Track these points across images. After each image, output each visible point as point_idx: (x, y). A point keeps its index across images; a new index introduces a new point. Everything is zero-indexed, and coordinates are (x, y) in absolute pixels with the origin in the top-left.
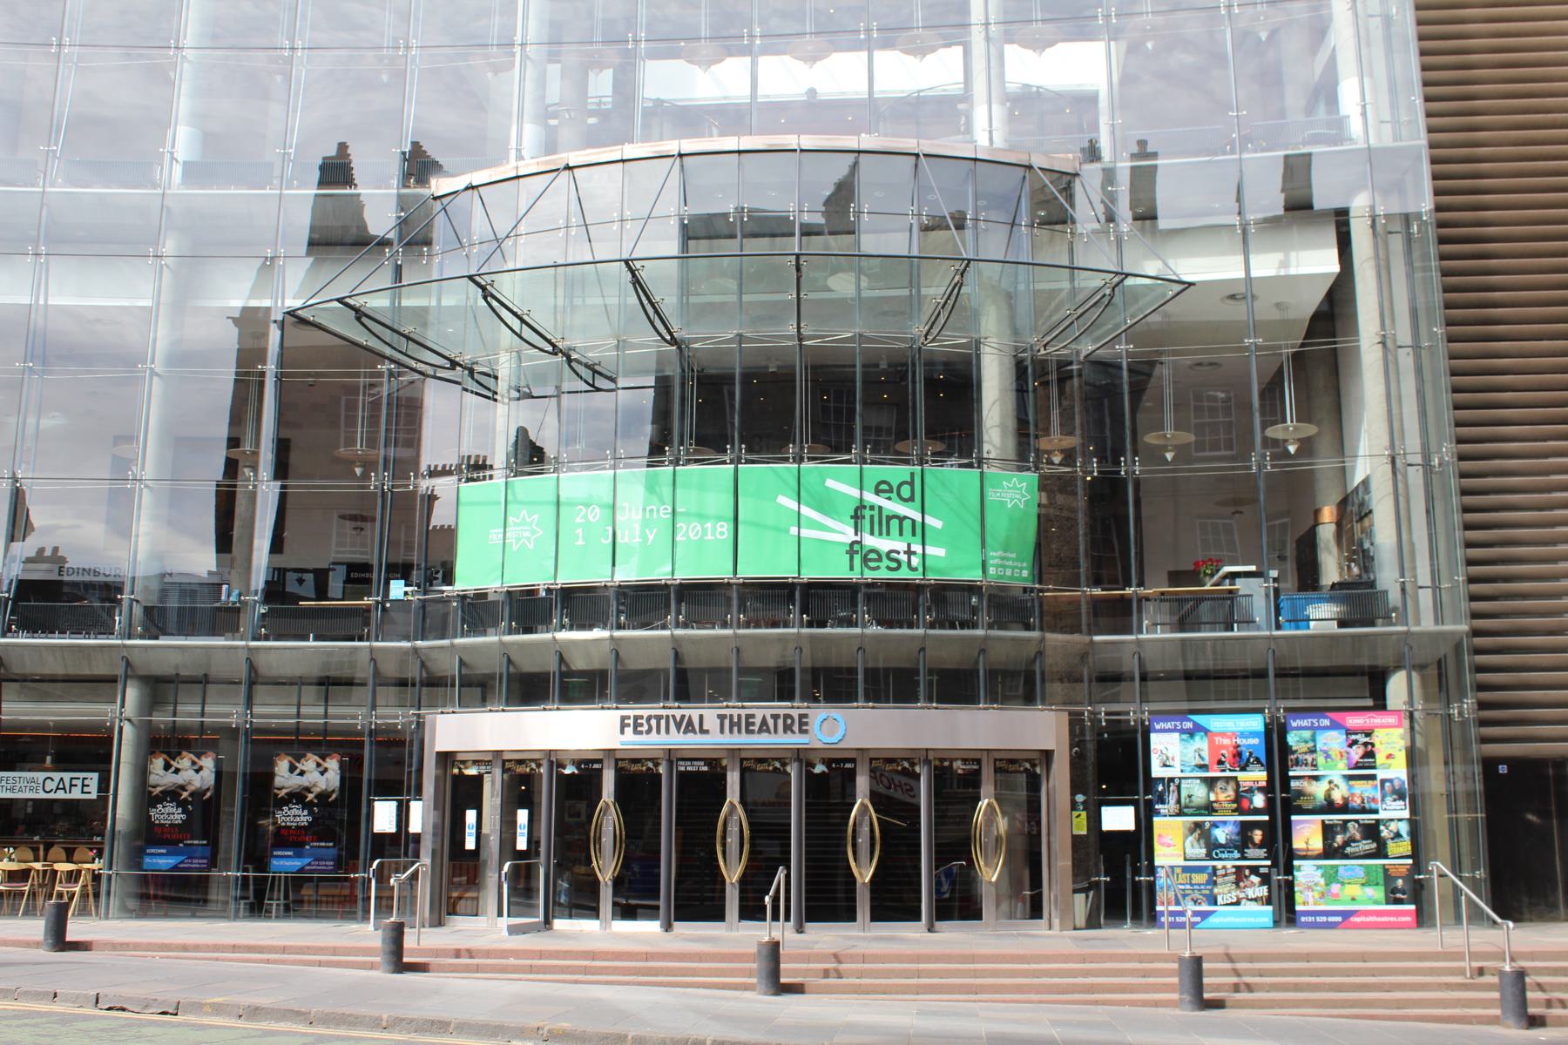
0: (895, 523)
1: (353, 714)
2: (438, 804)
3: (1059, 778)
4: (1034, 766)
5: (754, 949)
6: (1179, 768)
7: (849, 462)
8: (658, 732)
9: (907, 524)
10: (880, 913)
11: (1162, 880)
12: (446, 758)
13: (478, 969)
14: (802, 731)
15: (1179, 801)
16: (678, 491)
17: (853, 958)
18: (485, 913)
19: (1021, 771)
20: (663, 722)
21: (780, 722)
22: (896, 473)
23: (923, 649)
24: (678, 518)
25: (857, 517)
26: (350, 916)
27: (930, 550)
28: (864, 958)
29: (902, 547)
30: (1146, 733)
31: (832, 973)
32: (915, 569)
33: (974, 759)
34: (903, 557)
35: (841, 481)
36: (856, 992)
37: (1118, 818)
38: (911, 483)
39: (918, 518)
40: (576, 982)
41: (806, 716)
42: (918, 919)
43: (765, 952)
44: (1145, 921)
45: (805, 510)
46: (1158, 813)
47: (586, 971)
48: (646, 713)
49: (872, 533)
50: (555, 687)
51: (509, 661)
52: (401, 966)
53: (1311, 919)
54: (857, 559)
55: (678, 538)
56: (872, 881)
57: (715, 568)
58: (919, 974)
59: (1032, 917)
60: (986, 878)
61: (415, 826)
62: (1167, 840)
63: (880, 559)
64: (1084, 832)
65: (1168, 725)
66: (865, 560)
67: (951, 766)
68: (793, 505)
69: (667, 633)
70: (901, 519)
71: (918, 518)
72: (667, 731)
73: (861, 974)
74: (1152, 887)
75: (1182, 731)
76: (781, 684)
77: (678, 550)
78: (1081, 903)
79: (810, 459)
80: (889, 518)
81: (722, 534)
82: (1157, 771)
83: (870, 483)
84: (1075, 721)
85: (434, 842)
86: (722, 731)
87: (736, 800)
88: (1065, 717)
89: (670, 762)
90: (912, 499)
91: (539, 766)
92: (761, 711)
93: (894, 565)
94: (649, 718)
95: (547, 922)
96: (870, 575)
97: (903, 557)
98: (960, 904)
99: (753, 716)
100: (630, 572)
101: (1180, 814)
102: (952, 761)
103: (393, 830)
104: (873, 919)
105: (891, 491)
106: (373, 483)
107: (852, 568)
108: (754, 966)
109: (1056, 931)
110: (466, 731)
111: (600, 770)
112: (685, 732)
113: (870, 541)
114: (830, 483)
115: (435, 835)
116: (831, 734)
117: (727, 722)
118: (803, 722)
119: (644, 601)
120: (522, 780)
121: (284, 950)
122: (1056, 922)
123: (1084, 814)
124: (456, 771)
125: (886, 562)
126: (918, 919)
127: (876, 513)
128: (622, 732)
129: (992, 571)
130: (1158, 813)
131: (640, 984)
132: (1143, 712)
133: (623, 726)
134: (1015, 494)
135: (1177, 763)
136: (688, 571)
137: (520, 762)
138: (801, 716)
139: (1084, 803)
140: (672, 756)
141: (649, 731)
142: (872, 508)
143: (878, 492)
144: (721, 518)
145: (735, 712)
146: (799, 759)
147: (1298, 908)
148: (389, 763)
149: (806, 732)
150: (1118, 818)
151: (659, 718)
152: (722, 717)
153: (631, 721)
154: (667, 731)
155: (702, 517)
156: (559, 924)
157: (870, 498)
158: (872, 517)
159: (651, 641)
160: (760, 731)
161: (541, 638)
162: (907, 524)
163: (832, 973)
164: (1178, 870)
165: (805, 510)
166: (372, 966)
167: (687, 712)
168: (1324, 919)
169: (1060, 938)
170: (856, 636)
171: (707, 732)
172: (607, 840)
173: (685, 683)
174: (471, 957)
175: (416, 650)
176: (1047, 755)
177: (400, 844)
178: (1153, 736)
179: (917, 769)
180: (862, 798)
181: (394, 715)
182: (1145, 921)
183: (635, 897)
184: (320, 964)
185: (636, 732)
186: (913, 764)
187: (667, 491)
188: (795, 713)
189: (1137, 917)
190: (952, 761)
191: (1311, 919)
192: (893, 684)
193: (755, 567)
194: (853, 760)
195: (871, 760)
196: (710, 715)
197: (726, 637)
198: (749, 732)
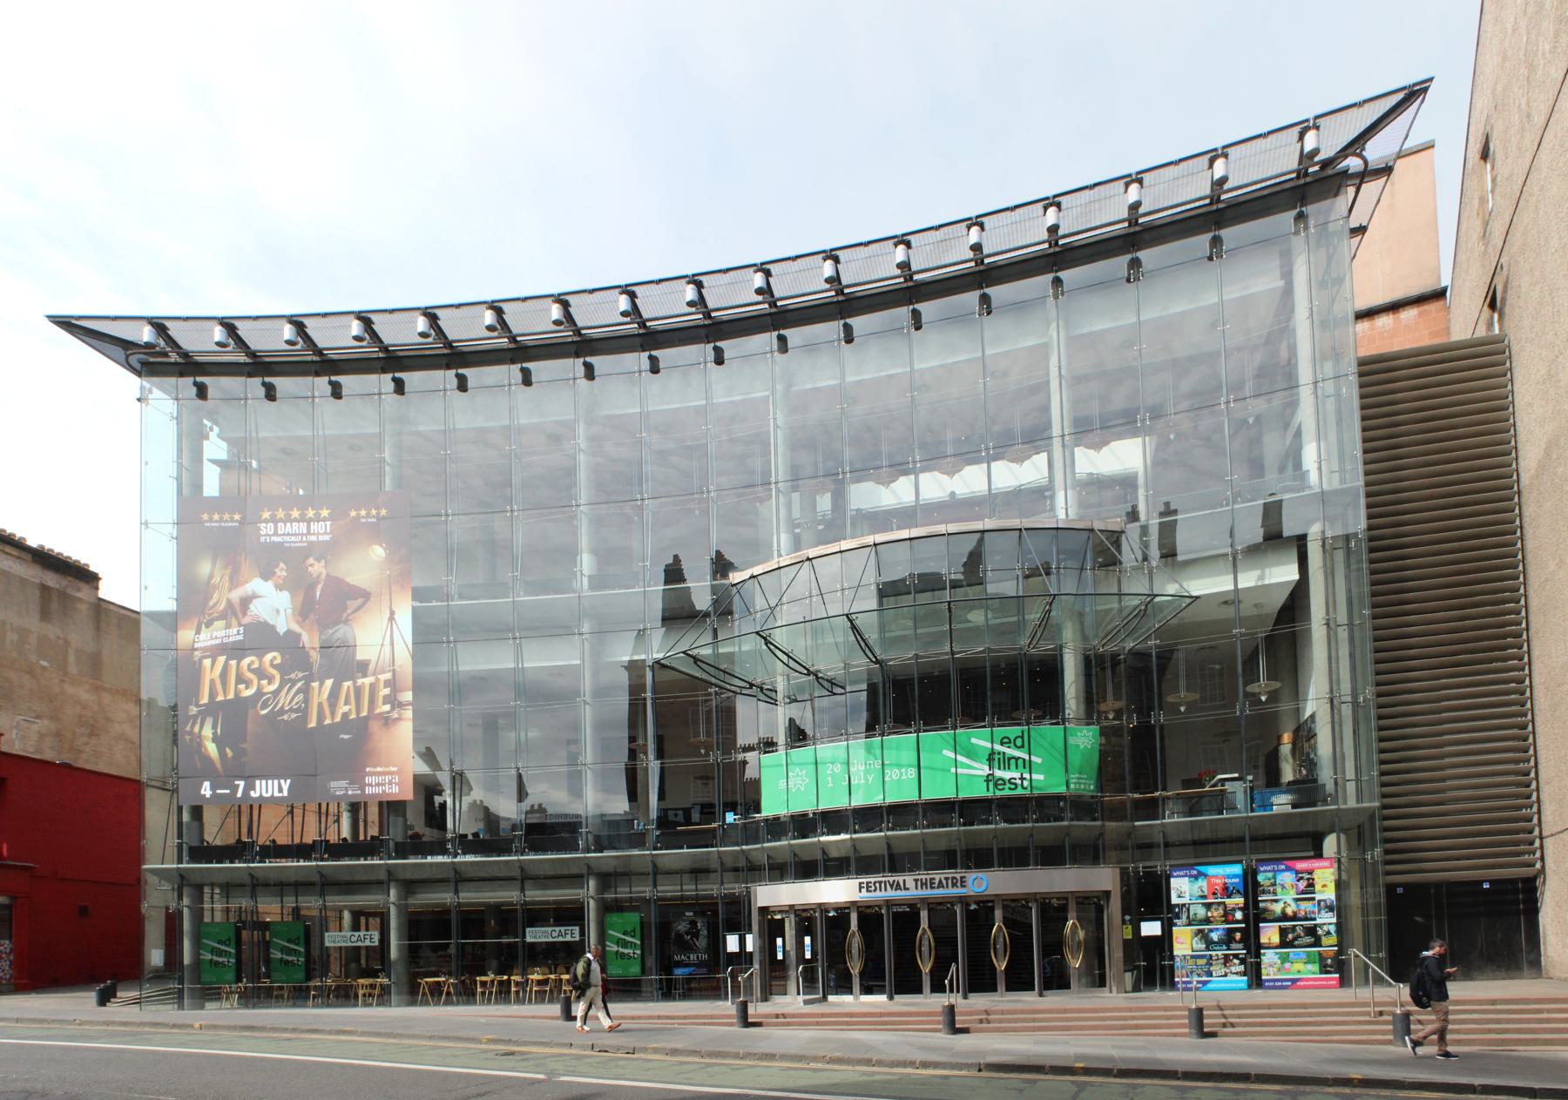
0: (1013, 762)
2: (761, 935)
10: (1011, 987)
11: (1178, 963)
13: (788, 1024)
17: (996, 1013)
19: (1092, 905)
22: (1013, 731)
25: (990, 759)
27: (1035, 776)
28: (1002, 1013)
29: (1018, 775)
33: (1064, 897)
35: (980, 739)
37: (1151, 928)
47: (847, 1023)
57: (908, 795)
61: (749, 948)
66: (996, 785)
70: (1017, 759)
73: (1001, 1021)
74: (1172, 968)
76: (948, 859)
82: (1175, 900)
83: (997, 738)
96: (998, 793)
104: (1008, 990)
109: (1114, 994)
110: (775, 895)
113: (998, 773)
114: (973, 740)
119: (868, 816)
120: (806, 918)
140: (889, 903)
143: (1002, 744)
148: (736, 915)
150: (1151, 928)
155: (899, 766)
156: (831, 998)
157: (998, 747)
172: (855, 951)
176: (1107, 894)
180: (924, 923)
187: (878, 752)
192: (1014, 857)
196: (909, 879)
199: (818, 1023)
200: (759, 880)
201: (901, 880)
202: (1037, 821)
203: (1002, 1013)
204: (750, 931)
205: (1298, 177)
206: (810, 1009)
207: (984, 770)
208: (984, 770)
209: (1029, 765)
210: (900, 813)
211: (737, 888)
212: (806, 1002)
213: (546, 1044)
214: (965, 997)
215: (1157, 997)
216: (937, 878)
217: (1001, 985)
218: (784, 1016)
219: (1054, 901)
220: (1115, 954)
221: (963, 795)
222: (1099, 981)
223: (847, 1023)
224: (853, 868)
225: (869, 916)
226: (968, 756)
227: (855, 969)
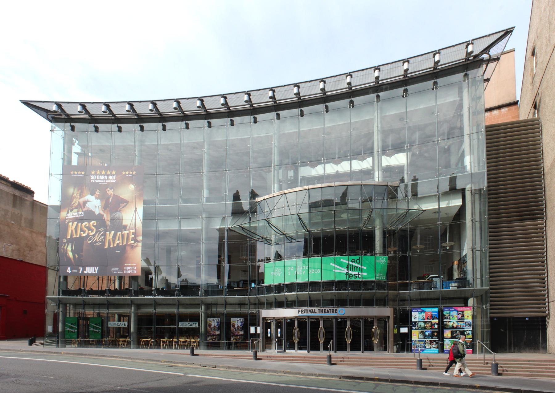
0: (356, 268)
2: (263, 328)
3: (391, 321)
10: (352, 349)
12: (264, 319)
13: (272, 360)
17: (346, 358)
19: (382, 321)
22: (356, 257)
25: (347, 267)
28: (349, 358)
29: (357, 273)
33: (372, 318)
35: (344, 259)
37: (404, 330)
47: (292, 360)
57: (317, 279)
61: (258, 332)
66: (349, 276)
68: (334, 265)
70: (357, 267)
73: (348, 361)
74: (411, 344)
76: (331, 302)
82: (413, 320)
83: (350, 260)
84: (395, 310)
96: (350, 279)
101: (418, 329)
113: (350, 272)
114: (342, 260)
119: (303, 286)
120: (279, 322)
133: (299, 312)
136: (312, 280)
140: (309, 318)
143: (352, 262)
148: (253, 320)
150: (404, 330)
155: (314, 268)
156: (287, 351)
157: (350, 263)
166: (251, 359)
172: (296, 335)
173: (312, 303)
176: (389, 317)
177: (256, 335)
187: (307, 263)
188: (334, 309)
193: (325, 279)
196: (317, 309)
200: (262, 308)
201: (313, 309)
205: (465, 61)
209: (361, 270)
210: (314, 285)
211: (254, 310)
214: (335, 352)
215: (405, 355)
216: (327, 309)
217: (349, 348)
219: (369, 319)
221: (338, 279)
223: (292, 360)
225: (302, 322)
227: (296, 341)
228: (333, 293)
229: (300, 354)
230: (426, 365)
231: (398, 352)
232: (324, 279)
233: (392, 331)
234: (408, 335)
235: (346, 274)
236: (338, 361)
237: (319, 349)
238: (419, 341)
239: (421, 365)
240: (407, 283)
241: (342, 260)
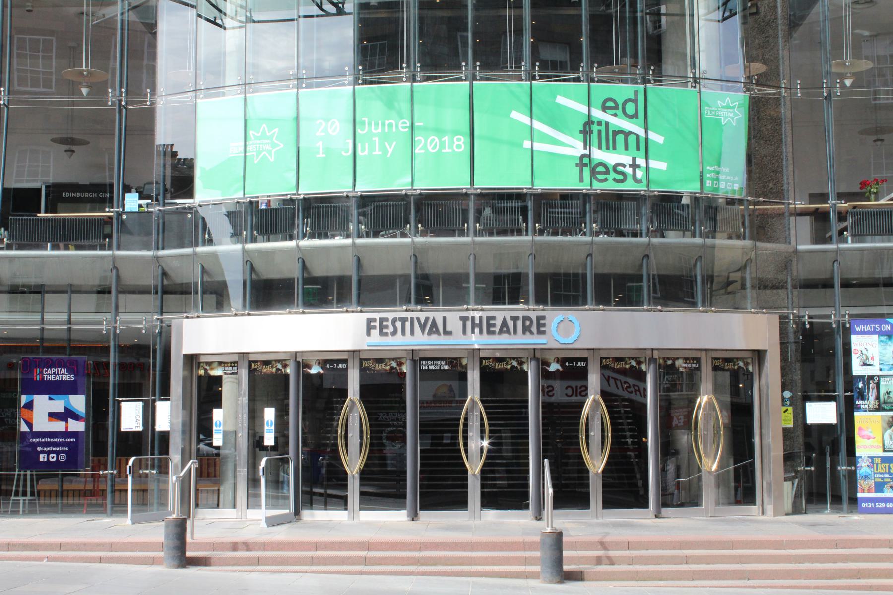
0: (620, 138)
1: (90, 319)
2: (186, 404)
3: (770, 379)
4: (747, 364)
5: (537, 539)
6: (878, 367)
7: (577, 80)
8: (403, 333)
9: (632, 139)
10: (490, 500)
11: (863, 468)
12: (191, 360)
13: (259, 561)
14: (540, 332)
15: (878, 397)
16: (416, 106)
17: (618, 546)
18: (152, 504)
19: (736, 374)
20: (408, 324)
21: (520, 324)
22: (622, 91)
23: (647, 256)
24: (416, 132)
25: (586, 132)
26: (100, 509)
27: (653, 164)
28: (629, 546)
29: (627, 160)
30: (847, 332)
31: (605, 561)
32: (640, 182)
33: (694, 358)
34: (629, 170)
35: (569, 98)
36: (632, 579)
37: (822, 413)
38: (635, 101)
39: (642, 133)
40: (361, 573)
41: (544, 318)
42: (646, 505)
43: (549, 541)
44: (845, 505)
45: (537, 125)
46: (859, 408)
47: (366, 561)
48: (391, 316)
49: (600, 148)
50: (299, 289)
51: (252, 269)
52: (186, 562)
53: (870, 505)
54: (587, 171)
55: (417, 151)
56: (603, 471)
57: (451, 178)
58: (687, 560)
59: (738, 502)
60: (705, 468)
61: (162, 424)
62: (864, 433)
63: (607, 172)
64: (791, 425)
65: (868, 328)
66: (593, 173)
67: (674, 364)
68: (526, 120)
69: (408, 240)
70: (627, 134)
71: (642, 133)
72: (412, 333)
73: (631, 561)
74: (852, 476)
75: (881, 333)
76: (504, 288)
77: (417, 162)
78: (788, 490)
79: (541, 77)
80: (616, 133)
81: (459, 146)
82: (857, 370)
83: (597, 100)
84: (783, 322)
85: (183, 440)
86: (464, 332)
87: (477, 397)
88: (776, 319)
89: (414, 362)
90: (636, 115)
91: (285, 366)
92: (502, 313)
93: (620, 177)
94: (394, 321)
95: (297, 513)
96: (598, 187)
97: (629, 170)
98: (681, 495)
99: (494, 318)
100: (371, 183)
101: (879, 408)
102: (675, 359)
103: (140, 429)
105: (616, 108)
106: (111, 98)
107: (582, 180)
108: (538, 554)
109: (128, 520)
110: (204, 335)
111: (346, 370)
112: (430, 333)
113: (598, 155)
114: (560, 100)
115: (183, 432)
116: (567, 335)
117: (469, 324)
118: (541, 326)
119: (384, 211)
120: (267, 380)
121: (60, 547)
122: (770, 508)
123: (791, 409)
124: (202, 372)
125: (613, 175)
126: (646, 505)
127: (603, 128)
128: (368, 334)
129: (708, 184)
130: (859, 408)
131: (850, 588)
132: (844, 316)
133: (369, 328)
134: (730, 110)
135: (876, 363)
136: (426, 182)
137: (267, 363)
138: (539, 318)
139: (791, 398)
140: (416, 357)
141: (394, 333)
142: (599, 124)
143: (604, 108)
144: (457, 133)
145: (477, 315)
146: (534, 358)
147: (859, 495)
148: (141, 367)
149: (544, 332)
150: (822, 413)
151: (403, 320)
152: (464, 319)
153: (377, 324)
154: (412, 333)
155: (439, 131)
156: (306, 514)
157: (598, 114)
158: (600, 132)
159: (396, 248)
160: (501, 332)
161: (306, 241)
162: (632, 139)
163: (605, 561)
164: (878, 460)
165: (537, 125)
166: (153, 561)
167: (431, 315)
168: (883, 505)
169: (773, 521)
170: (586, 244)
171: (450, 333)
173: (426, 288)
174: (248, 550)
175: (157, 258)
176: (759, 355)
177: (148, 444)
178: (854, 338)
179: (643, 367)
180: (593, 397)
181: (136, 319)
182: (845, 505)
183: (383, 487)
184: (101, 560)
185: (382, 333)
186: (639, 363)
187: (405, 106)
188: (533, 316)
189: (837, 499)
190: (675, 359)
191: (870, 505)
192: (619, 289)
193: (490, 178)
194: (585, 360)
195: (602, 358)
196: (453, 317)
197: (464, 244)
198: (490, 332)
199: (312, 561)
200: (183, 309)
202: (477, 233)
203: (629, 546)
204: (165, 394)
206: (282, 533)
207: (577, 148)
208: (577, 148)
209: (644, 146)
210: (434, 210)
212: (272, 522)
213: (870, 588)
214: (414, 516)
215: (827, 520)
217: (709, 493)
218: (247, 546)
219: (680, 363)
220: (769, 447)
221: (543, 184)
222: (742, 489)
223: (366, 561)
224: (440, 293)
226: (552, 123)
227: (353, 462)
228: (524, 247)
229: (369, 525)
230: (579, 560)
231: (796, 510)
232: (487, 181)
233: (773, 421)
234: (836, 442)
235: (583, 162)
236: (587, 560)
237: (342, 502)
238: (884, 460)
239: (558, 561)
240: (149, 233)
241: (560, 100)
